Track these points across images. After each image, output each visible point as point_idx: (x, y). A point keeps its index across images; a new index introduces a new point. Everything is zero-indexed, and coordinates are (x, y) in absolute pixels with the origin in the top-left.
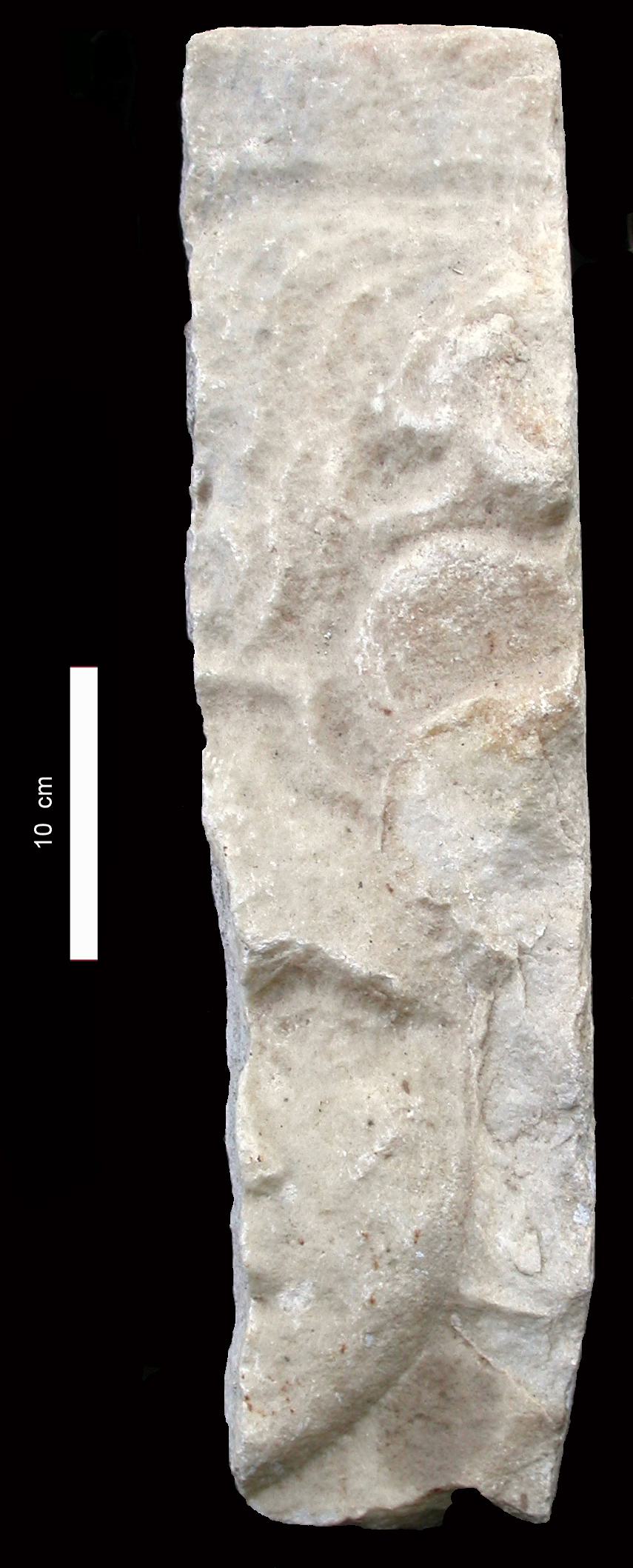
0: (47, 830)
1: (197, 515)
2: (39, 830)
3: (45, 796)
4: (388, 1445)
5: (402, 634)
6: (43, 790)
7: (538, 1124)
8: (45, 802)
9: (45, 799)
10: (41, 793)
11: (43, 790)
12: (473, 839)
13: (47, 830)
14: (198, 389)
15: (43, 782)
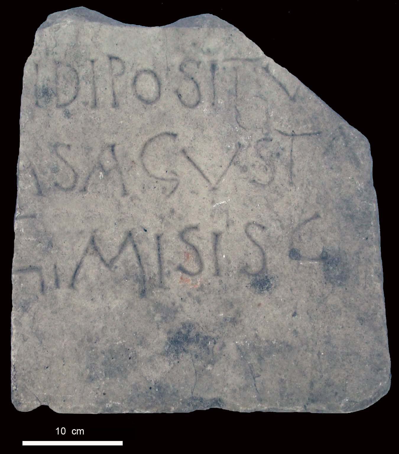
0: (63, 432)
1: (367, 405)
2: (63, 429)
3: (76, 432)
4: (178, 140)
5: (121, 122)
6: (79, 431)
7: (73, 253)
8: (74, 432)
9: (75, 432)
10: (77, 430)
11: (79, 431)
12: (252, 210)
13: (63, 432)
14: (296, 224)
15: (82, 431)
